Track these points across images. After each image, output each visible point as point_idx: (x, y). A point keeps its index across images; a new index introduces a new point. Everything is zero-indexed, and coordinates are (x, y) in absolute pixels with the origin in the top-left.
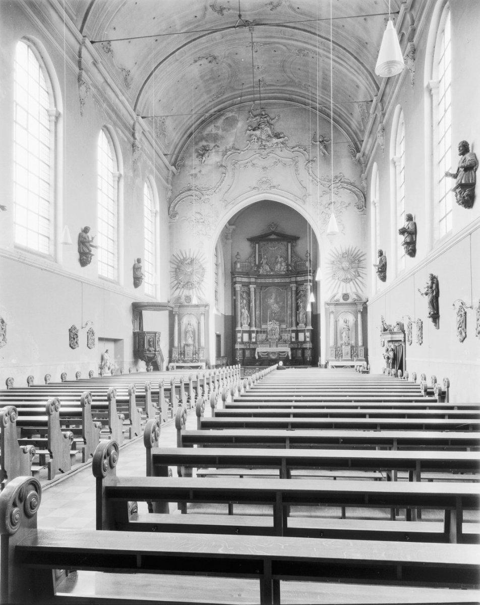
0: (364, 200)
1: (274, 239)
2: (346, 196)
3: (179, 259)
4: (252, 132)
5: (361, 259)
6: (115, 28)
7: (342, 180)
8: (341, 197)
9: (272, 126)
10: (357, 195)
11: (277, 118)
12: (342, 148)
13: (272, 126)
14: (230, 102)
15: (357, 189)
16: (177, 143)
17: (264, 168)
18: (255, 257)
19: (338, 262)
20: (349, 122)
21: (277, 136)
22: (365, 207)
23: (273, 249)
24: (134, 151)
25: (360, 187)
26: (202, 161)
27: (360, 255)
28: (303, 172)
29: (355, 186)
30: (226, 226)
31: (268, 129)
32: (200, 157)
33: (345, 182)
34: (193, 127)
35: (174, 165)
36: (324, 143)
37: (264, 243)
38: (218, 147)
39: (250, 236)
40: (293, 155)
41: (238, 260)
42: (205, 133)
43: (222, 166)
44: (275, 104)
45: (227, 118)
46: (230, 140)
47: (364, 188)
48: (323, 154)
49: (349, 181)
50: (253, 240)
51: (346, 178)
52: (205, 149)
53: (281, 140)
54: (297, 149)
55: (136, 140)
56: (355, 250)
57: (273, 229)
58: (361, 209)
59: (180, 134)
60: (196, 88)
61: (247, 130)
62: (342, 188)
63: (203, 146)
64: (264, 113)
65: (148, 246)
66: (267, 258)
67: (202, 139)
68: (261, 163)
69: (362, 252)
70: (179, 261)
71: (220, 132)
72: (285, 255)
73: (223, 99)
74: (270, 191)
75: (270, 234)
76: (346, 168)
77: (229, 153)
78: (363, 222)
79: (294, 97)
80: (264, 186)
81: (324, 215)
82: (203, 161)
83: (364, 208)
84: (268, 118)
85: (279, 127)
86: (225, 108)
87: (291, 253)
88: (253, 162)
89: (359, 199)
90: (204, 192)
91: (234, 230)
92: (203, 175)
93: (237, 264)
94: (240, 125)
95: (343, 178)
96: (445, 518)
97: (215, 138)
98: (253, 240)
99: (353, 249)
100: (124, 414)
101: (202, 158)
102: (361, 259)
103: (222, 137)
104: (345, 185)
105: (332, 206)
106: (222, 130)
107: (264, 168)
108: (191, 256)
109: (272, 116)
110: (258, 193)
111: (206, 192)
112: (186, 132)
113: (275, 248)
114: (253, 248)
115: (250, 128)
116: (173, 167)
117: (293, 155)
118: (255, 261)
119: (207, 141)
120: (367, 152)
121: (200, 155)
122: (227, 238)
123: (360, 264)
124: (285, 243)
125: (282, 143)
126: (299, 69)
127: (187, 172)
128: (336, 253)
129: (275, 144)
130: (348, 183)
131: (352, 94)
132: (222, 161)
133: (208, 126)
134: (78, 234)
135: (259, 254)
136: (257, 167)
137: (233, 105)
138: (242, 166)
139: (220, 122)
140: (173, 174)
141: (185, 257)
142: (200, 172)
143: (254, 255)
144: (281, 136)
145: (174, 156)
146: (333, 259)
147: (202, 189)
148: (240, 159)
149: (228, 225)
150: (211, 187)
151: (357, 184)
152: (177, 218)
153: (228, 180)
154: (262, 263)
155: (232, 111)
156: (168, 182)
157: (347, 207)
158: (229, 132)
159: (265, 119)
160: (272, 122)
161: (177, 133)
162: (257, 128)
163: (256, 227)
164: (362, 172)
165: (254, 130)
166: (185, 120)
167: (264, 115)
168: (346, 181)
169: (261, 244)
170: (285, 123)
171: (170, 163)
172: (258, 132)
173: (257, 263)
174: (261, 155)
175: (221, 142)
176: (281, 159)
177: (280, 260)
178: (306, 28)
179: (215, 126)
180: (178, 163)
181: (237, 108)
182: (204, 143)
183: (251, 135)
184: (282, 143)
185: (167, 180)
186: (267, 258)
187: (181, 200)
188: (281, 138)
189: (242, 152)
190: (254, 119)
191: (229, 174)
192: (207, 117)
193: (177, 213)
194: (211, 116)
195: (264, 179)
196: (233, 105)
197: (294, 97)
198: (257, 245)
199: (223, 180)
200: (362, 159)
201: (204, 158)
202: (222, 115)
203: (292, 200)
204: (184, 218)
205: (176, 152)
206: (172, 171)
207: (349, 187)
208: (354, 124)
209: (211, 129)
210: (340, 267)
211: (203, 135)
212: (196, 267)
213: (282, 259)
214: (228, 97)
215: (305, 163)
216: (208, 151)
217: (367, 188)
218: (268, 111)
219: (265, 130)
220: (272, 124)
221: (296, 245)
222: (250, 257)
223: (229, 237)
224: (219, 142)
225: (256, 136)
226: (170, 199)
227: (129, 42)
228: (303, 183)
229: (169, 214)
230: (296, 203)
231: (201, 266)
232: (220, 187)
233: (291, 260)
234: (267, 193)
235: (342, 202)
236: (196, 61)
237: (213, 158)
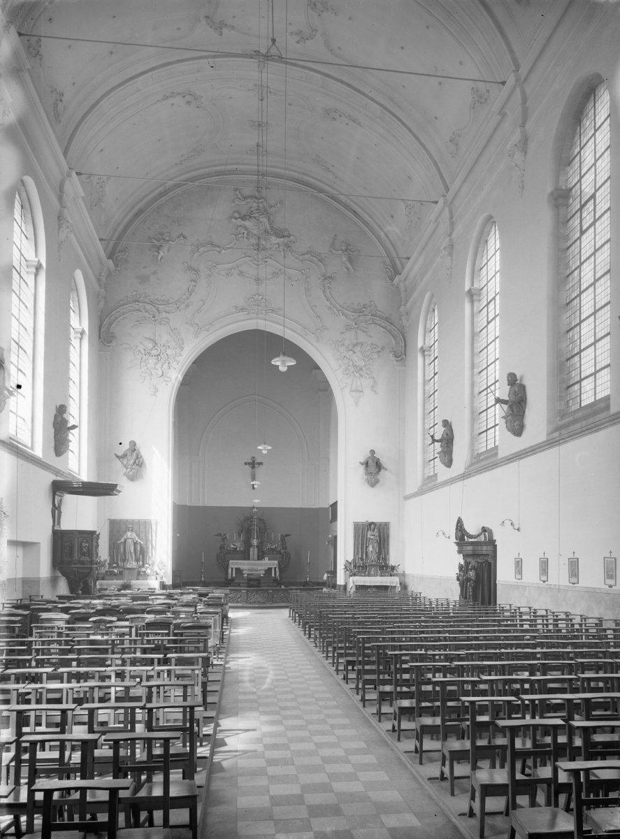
4: (240, 222)
6: (50, 19)
17: (258, 280)
21: (280, 234)
24: (60, 227)
55: (65, 210)
60: (159, 140)
65: (73, 391)
76: (377, 292)
82: (159, 258)
83: (404, 356)
89: (397, 343)
96: (19, 804)
105: (358, 349)
111: (164, 306)
112: (132, 208)
115: (236, 215)
126: (322, 138)
130: (381, 318)
134: (506, 430)
144: (286, 234)
156: (100, 285)
178: (345, 79)
180: (116, 251)
185: (99, 280)
190: (244, 203)
201: (161, 253)
226: (102, 311)
227: (70, 47)
229: (100, 337)
230: (305, 338)
236: (166, 98)
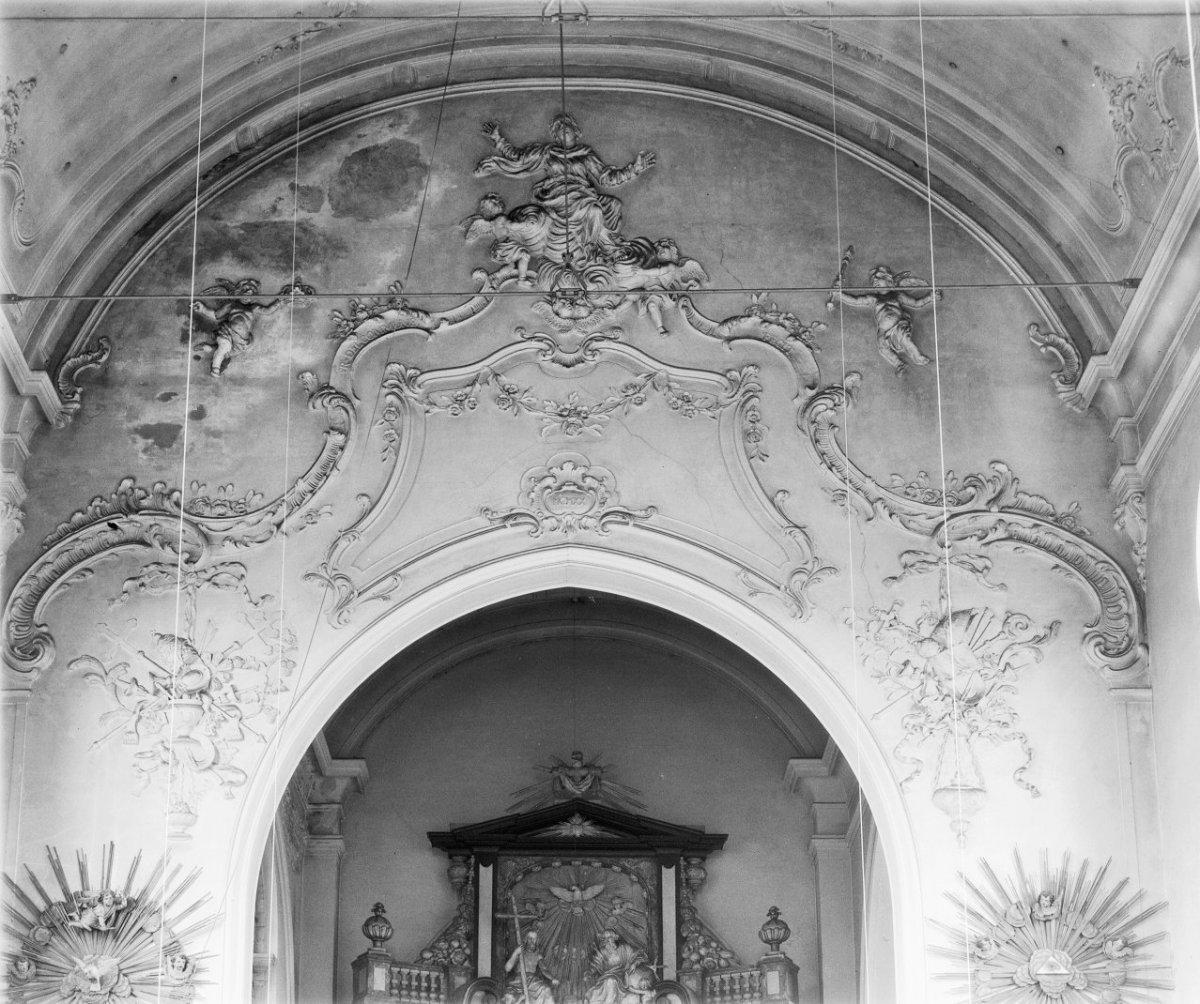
0: (1134, 608)
1: (583, 838)
2: (1027, 582)
3: (41, 905)
4: (502, 227)
5: (1140, 932)
7: (1008, 499)
8: (1003, 586)
9: (615, 206)
10: (1092, 579)
11: (638, 167)
12: (1004, 327)
13: (615, 206)
14: (387, 69)
15: (1090, 549)
16: (77, 252)
17: (570, 416)
18: (473, 937)
19: (1005, 948)
20: (1035, 198)
21: (644, 255)
22: (1146, 647)
23: (578, 893)
25: (1107, 544)
26: (211, 358)
27: (1134, 913)
28: (791, 458)
29: (1080, 534)
30: (312, 749)
31: (596, 214)
32: (203, 337)
33: (1029, 512)
34: (198, 162)
35: (52, 367)
36: (903, 309)
37: (529, 861)
38: (308, 291)
39: (443, 822)
40: (729, 355)
41: (380, 949)
42: (236, 220)
43: (324, 390)
44: (627, 99)
45: (365, 152)
46: (381, 264)
47: (1129, 546)
48: (894, 361)
49: (1046, 506)
50: (460, 844)
51: (1021, 487)
52: (236, 306)
53: (665, 275)
54: (747, 324)
56: (1097, 884)
57: (578, 790)
58: (1119, 654)
59: (99, 208)
61: (473, 218)
62: (1010, 538)
63: (225, 285)
64: (569, 140)
66: (541, 948)
67: (213, 249)
68: (549, 386)
69: (1140, 896)
70: (39, 914)
71: (322, 218)
72: (641, 935)
73: (345, 51)
74: (603, 540)
75: (562, 815)
76: (1021, 435)
77: (372, 325)
78: (1138, 728)
79: (738, 67)
80: (571, 510)
81: (914, 683)
82: (217, 362)
83: (1140, 650)
84: (593, 166)
85: (654, 207)
86: (353, 103)
87: (680, 922)
88: (503, 379)
90: (214, 524)
91: (357, 787)
92: (216, 434)
93: (368, 972)
94: (435, 188)
95: (1011, 491)
97: (290, 247)
98: (460, 844)
99: (1090, 877)
100: (613, 977)
101: (215, 346)
102: (1140, 932)
103: (336, 246)
104: (1024, 525)
105: (954, 633)
106: (335, 207)
107: (570, 416)
108: (117, 884)
109: (614, 154)
110: (531, 542)
113: (590, 893)
114: (460, 889)
116: (44, 379)
117: (729, 355)
118: (474, 958)
119: (244, 258)
120: (1150, 347)
121: (201, 323)
122: (314, 830)
123: (1132, 964)
124: (645, 865)
125: (673, 291)
127: (122, 415)
128: (978, 906)
129: (632, 297)
131: (646, 510)
132: (328, 365)
133: (259, 186)
135: (495, 923)
136: (530, 408)
137: (397, 89)
138: (444, 398)
139: (323, 171)
140: (36, 423)
141: (74, 886)
142: (198, 414)
143: (463, 930)
144: (665, 255)
145: (64, 307)
146: (972, 930)
147: (207, 511)
148: (434, 361)
149: (324, 753)
150: (257, 501)
151: (1089, 519)
152: (45, 661)
153: (357, 469)
154: (514, 973)
155: (398, 117)
157: (1039, 639)
158: (375, 223)
159: (577, 168)
160: (612, 185)
161: (77, 201)
162: (530, 210)
163: (488, 768)
164: (1112, 462)
165: (514, 216)
166: (133, 133)
167: (573, 148)
168: (1029, 501)
169: (511, 865)
170: (699, 198)
171: (26, 355)
172: (534, 231)
173: (485, 968)
174: (554, 345)
175: (327, 270)
176: (663, 371)
177: (614, 958)
179: (292, 187)
181: (423, 108)
182: (229, 269)
183: (494, 245)
184: (673, 291)
186: (541, 948)
187: (71, 565)
188: (665, 263)
189: (445, 327)
190: (518, 166)
191: (371, 433)
192: (250, 138)
193: (46, 638)
194: (280, 132)
195: (568, 472)
196: (397, 89)
197: (738, 67)
198: (486, 874)
199: (332, 464)
200: (1112, 390)
201: (225, 346)
202: (337, 135)
203: (730, 594)
204: (83, 666)
205: (75, 288)
206: (35, 400)
207: (1049, 539)
208: (1065, 219)
209: (273, 201)
210: (1021, 976)
211: (223, 232)
212: (148, 951)
213: (629, 952)
214: (377, 42)
215: (800, 402)
216: (249, 307)
217: (1152, 539)
218: (593, 125)
219: (579, 222)
220: (612, 197)
221: (703, 881)
222: (446, 935)
223: (329, 822)
224: (318, 269)
225: (524, 245)
228: (789, 503)
231: (172, 948)
232: (312, 503)
233: (680, 961)
234: (579, 545)
235: (1009, 614)
237: (281, 347)
